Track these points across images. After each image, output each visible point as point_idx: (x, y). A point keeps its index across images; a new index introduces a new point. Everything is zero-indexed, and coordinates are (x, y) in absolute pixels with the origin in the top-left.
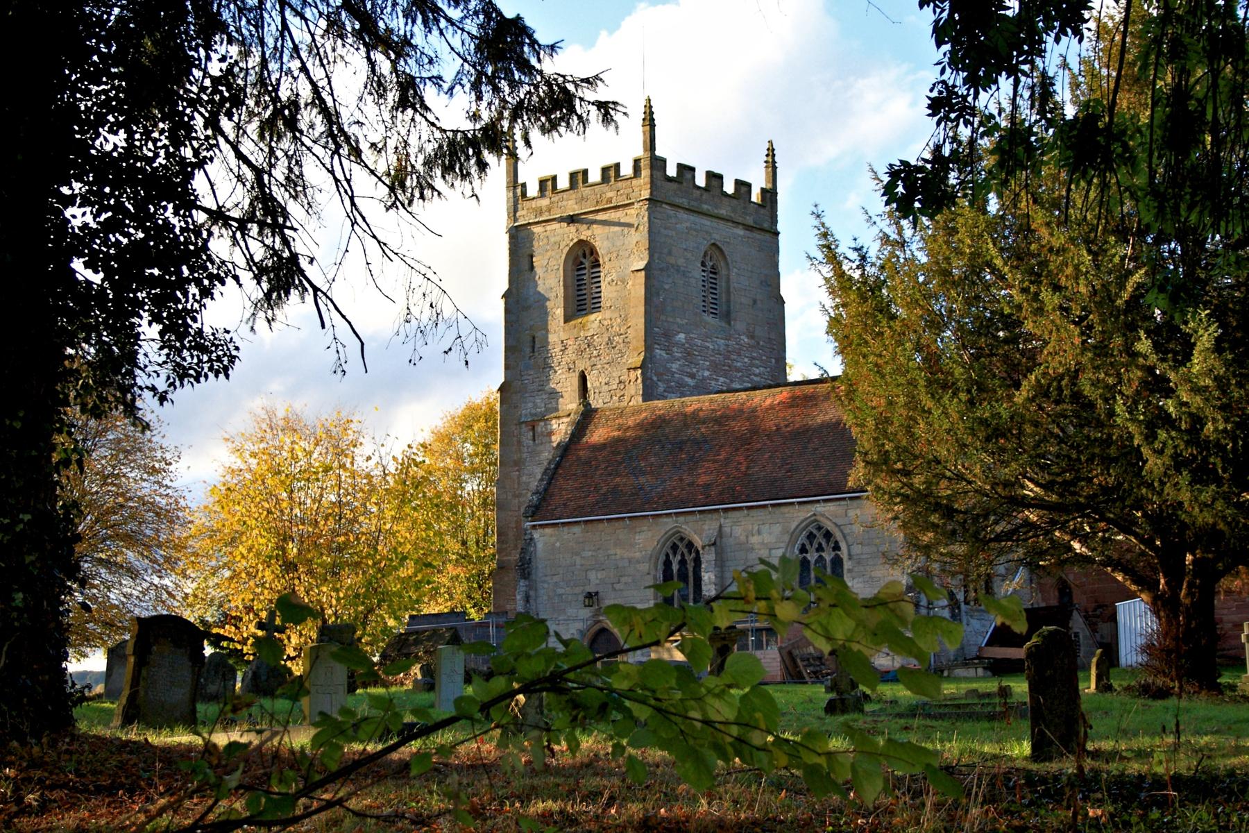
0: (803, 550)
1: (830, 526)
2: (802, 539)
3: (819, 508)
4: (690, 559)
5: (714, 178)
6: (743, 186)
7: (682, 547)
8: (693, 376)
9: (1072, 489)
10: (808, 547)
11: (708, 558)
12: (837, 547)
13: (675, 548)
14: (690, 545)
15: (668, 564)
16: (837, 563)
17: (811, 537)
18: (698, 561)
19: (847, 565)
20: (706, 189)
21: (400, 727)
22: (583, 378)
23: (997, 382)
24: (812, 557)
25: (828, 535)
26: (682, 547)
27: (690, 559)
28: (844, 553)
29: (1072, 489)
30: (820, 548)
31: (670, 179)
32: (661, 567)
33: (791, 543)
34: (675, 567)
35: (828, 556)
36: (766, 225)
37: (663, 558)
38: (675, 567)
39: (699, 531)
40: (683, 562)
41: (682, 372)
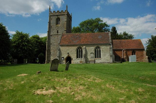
0: (96, 49)
4: (99, 50)
12: (100, 49)
15: (78, 50)
16: (100, 51)
18: (82, 50)
19: (101, 51)
22: (58, 31)
27: (99, 50)
28: (101, 50)
40: (80, 50)
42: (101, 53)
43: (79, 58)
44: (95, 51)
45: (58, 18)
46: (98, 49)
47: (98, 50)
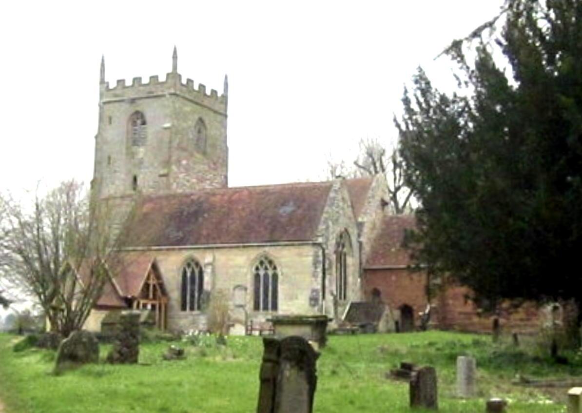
0: (257, 269)
1: (272, 258)
2: (257, 263)
3: (267, 249)
4: (197, 271)
5: (202, 87)
6: (214, 92)
7: (193, 265)
8: (188, 181)
9: (52, 266)
10: (260, 267)
11: (208, 271)
12: (275, 268)
13: (189, 265)
14: (197, 264)
15: (185, 273)
16: (275, 277)
17: (262, 263)
19: (280, 278)
20: (198, 92)
21: (383, 297)
23: (117, 182)
24: (262, 272)
25: (271, 262)
26: (193, 265)
27: (197, 271)
28: (279, 271)
29: (52, 266)
30: (266, 269)
31: (182, 85)
32: (181, 274)
33: (252, 265)
34: (189, 275)
35: (270, 272)
36: (222, 111)
37: (182, 269)
38: (189, 275)
39: (197, 255)
40: (193, 273)
41: (184, 179)
42: (280, 288)
43: (196, 312)
44: (257, 276)
45: (137, 113)
46: (266, 269)
47: (266, 275)
